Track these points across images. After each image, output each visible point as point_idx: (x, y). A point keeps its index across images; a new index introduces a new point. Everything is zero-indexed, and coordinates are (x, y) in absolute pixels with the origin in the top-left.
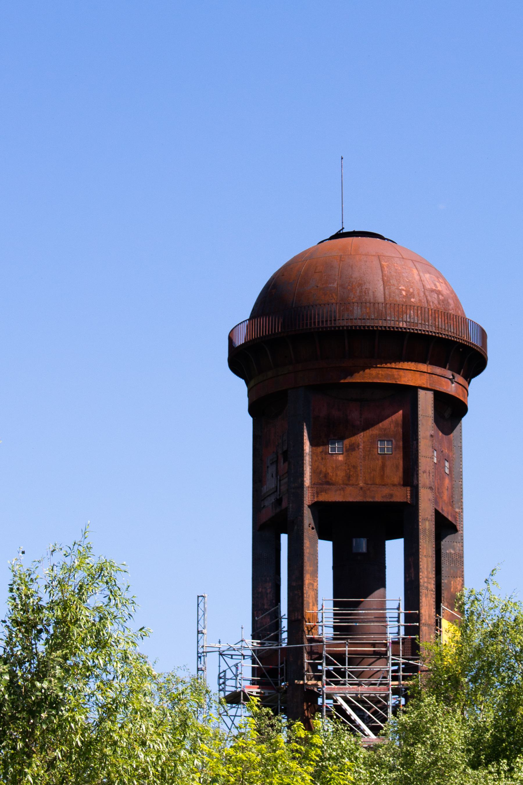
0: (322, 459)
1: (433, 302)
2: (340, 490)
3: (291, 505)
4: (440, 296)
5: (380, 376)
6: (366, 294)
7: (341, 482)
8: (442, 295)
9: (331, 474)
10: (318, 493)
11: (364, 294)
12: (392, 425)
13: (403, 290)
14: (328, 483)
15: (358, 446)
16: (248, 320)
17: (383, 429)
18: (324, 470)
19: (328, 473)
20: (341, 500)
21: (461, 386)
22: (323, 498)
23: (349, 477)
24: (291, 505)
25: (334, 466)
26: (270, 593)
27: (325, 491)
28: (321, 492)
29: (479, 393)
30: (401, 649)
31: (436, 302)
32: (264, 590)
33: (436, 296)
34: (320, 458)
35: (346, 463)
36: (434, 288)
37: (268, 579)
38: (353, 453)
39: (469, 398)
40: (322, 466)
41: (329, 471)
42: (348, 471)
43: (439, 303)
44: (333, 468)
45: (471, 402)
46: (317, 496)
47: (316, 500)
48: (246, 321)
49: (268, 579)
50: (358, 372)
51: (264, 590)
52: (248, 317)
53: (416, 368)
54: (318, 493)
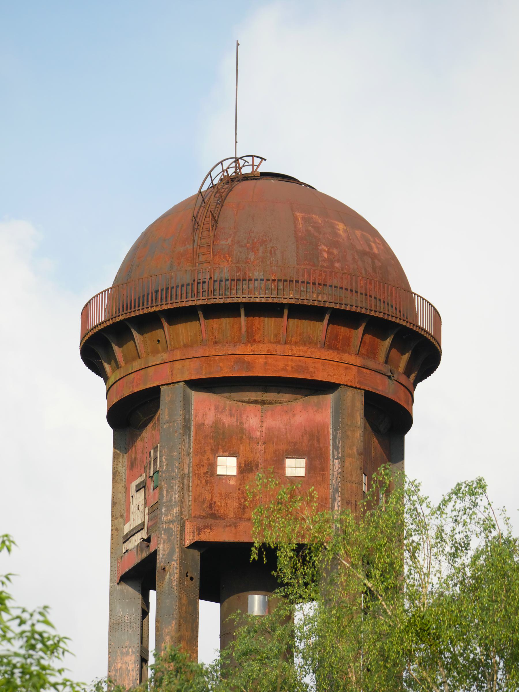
0: (207, 482)
1: (365, 269)
2: (230, 526)
3: (162, 546)
4: (376, 261)
5: (289, 368)
6: (271, 254)
7: (231, 515)
8: (379, 260)
9: (219, 504)
10: (199, 530)
11: (268, 254)
12: (305, 438)
13: (325, 251)
14: (214, 516)
15: (257, 466)
16: (111, 288)
17: (293, 442)
18: (209, 497)
19: (215, 503)
20: (232, 540)
21: (402, 387)
22: (208, 536)
23: (244, 509)
24: (162, 546)
25: (223, 493)
26: (133, 670)
27: (210, 527)
28: (205, 528)
29: (428, 398)
30: (331, 443)
31: (370, 269)
32: (124, 667)
33: (370, 261)
34: (204, 481)
35: (239, 489)
36: (368, 250)
37: (130, 650)
38: (250, 475)
39: (414, 407)
40: (207, 493)
41: (216, 499)
42: (243, 500)
43: (374, 270)
44: (221, 494)
45: (418, 411)
46: (199, 534)
47: (196, 539)
48: (108, 290)
49: (130, 650)
50: (277, 557)
51: (124, 667)
52: (111, 286)
53: (341, 359)
54: (199, 530)
